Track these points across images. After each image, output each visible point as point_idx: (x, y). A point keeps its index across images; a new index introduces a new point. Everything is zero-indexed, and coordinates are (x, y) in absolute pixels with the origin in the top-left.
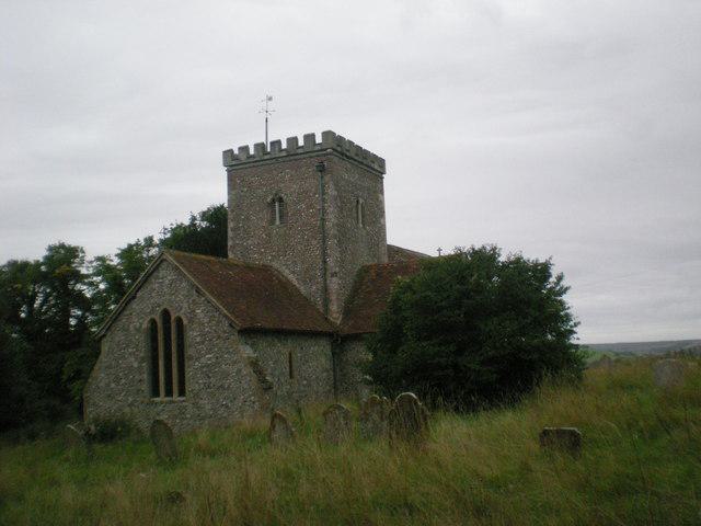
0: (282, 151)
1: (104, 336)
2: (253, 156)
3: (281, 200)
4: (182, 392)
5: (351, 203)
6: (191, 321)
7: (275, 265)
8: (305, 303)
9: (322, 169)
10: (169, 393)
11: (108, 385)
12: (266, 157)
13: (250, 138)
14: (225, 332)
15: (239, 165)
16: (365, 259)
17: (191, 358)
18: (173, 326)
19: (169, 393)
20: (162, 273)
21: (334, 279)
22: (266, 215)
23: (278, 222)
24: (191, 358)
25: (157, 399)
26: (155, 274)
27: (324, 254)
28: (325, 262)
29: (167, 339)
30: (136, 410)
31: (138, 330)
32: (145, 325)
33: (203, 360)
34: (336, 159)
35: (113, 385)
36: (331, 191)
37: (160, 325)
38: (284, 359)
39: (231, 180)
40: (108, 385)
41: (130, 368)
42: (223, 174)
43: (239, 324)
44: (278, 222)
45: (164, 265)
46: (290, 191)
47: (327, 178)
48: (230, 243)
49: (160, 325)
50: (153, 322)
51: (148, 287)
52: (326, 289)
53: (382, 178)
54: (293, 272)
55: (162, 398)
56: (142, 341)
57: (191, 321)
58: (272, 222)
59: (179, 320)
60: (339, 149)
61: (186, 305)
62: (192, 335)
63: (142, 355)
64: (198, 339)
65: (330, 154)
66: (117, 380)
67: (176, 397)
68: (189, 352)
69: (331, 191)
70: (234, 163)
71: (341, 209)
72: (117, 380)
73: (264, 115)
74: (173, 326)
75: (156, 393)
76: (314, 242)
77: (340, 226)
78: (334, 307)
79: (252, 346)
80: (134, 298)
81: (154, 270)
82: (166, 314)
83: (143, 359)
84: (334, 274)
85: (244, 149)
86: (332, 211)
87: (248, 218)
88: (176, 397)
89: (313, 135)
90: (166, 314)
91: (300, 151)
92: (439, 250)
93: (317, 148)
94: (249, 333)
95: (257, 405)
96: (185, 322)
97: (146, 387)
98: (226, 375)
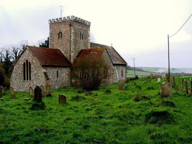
0: (62, 20)
1: (14, 65)
2: (55, 22)
3: (61, 33)
4: (30, 80)
5: (78, 34)
6: (32, 63)
7: (59, 49)
9: (70, 25)
10: (27, 80)
11: (15, 77)
12: (58, 22)
13: (57, 16)
15: (54, 24)
16: (82, 47)
17: (32, 71)
18: (29, 63)
19: (27, 80)
20: (26, 51)
21: (72, 53)
26: (25, 51)
28: (70, 49)
29: (27, 66)
30: (21, 83)
31: (21, 64)
34: (74, 23)
35: (16, 77)
36: (73, 31)
37: (26, 63)
38: (56, 72)
41: (20, 73)
45: (27, 49)
46: (63, 30)
47: (72, 28)
49: (26, 63)
50: (24, 63)
51: (24, 54)
52: (70, 56)
53: (90, 27)
54: (63, 51)
56: (22, 66)
57: (32, 63)
58: (59, 38)
59: (30, 62)
60: (75, 20)
61: (31, 59)
62: (32, 66)
63: (22, 70)
65: (73, 21)
66: (17, 76)
67: (29, 81)
68: (32, 70)
69: (73, 31)
71: (75, 35)
72: (17, 76)
74: (29, 63)
75: (25, 80)
76: (68, 43)
77: (75, 40)
78: (72, 60)
82: (27, 61)
84: (72, 52)
87: (54, 37)
88: (29, 81)
90: (27, 61)
92: (112, 44)
93: (70, 20)
94: (44, 66)
96: (31, 63)
97: (22, 78)
98: (39, 76)
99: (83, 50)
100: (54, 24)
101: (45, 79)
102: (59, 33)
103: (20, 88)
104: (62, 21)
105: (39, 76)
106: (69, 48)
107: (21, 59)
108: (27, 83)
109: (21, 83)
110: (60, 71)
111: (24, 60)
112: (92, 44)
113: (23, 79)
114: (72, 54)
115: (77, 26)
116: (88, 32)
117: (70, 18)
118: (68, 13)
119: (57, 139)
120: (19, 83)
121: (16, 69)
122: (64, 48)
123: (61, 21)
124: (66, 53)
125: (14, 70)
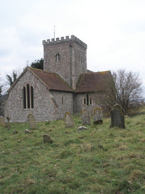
0: (59, 41)
1: (10, 91)
3: (59, 55)
4: (32, 107)
6: (35, 87)
8: (66, 83)
9: (71, 46)
10: (29, 107)
11: (11, 105)
12: (55, 42)
14: (45, 90)
15: (48, 45)
17: (35, 98)
19: (29, 107)
22: (54, 59)
23: (58, 61)
24: (35, 98)
25: (25, 109)
27: (71, 70)
30: (19, 112)
31: (20, 90)
32: (22, 88)
33: (39, 98)
35: (13, 105)
36: (73, 52)
37: (26, 88)
38: (61, 98)
39: (45, 49)
40: (11, 105)
42: (42, 48)
43: (49, 88)
44: (58, 61)
46: (61, 53)
47: (72, 49)
48: (44, 67)
49: (26, 88)
50: (24, 87)
52: (71, 80)
53: (86, 50)
54: (62, 75)
55: (27, 109)
56: (21, 92)
58: (56, 61)
59: (32, 87)
60: (75, 40)
61: (34, 83)
62: (35, 91)
64: (37, 92)
67: (31, 109)
68: (35, 96)
69: (73, 52)
70: (46, 44)
73: (54, 31)
76: (68, 67)
77: (75, 62)
79: (52, 94)
80: (19, 80)
81: (25, 72)
82: (28, 85)
83: (21, 98)
84: (74, 76)
85: (49, 40)
86: (73, 60)
88: (31, 109)
89: (63, 37)
90: (28, 85)
91: (65, 41)
94: (52, 91)
95: (54, 111)
96: (33, 87)
97: (22, 106)
98: (45, 102)
99: (82, 75)
100: (48, 45)
101: (54, 105)
102: (57, 55)
103: (18, 119)
104: (60, 42)
105: (45, 102)
106: (70, 72)
107: (19, 83)
108: (29, 111)
109: (19, 112)
110: (64, 98)
111: (24, 84)
112: (88, 71)
113: (22, 108)
114: (74, 78)
115: (76, 46)
116: (85, 55)
117: (55, 40)
118: (62, 33)
119: (121, 149)
120: (17, 112)
121: (12, 96)
122: (62, 72)
123: (58, 42)
124: (66, 77)
125: (10, 97)
